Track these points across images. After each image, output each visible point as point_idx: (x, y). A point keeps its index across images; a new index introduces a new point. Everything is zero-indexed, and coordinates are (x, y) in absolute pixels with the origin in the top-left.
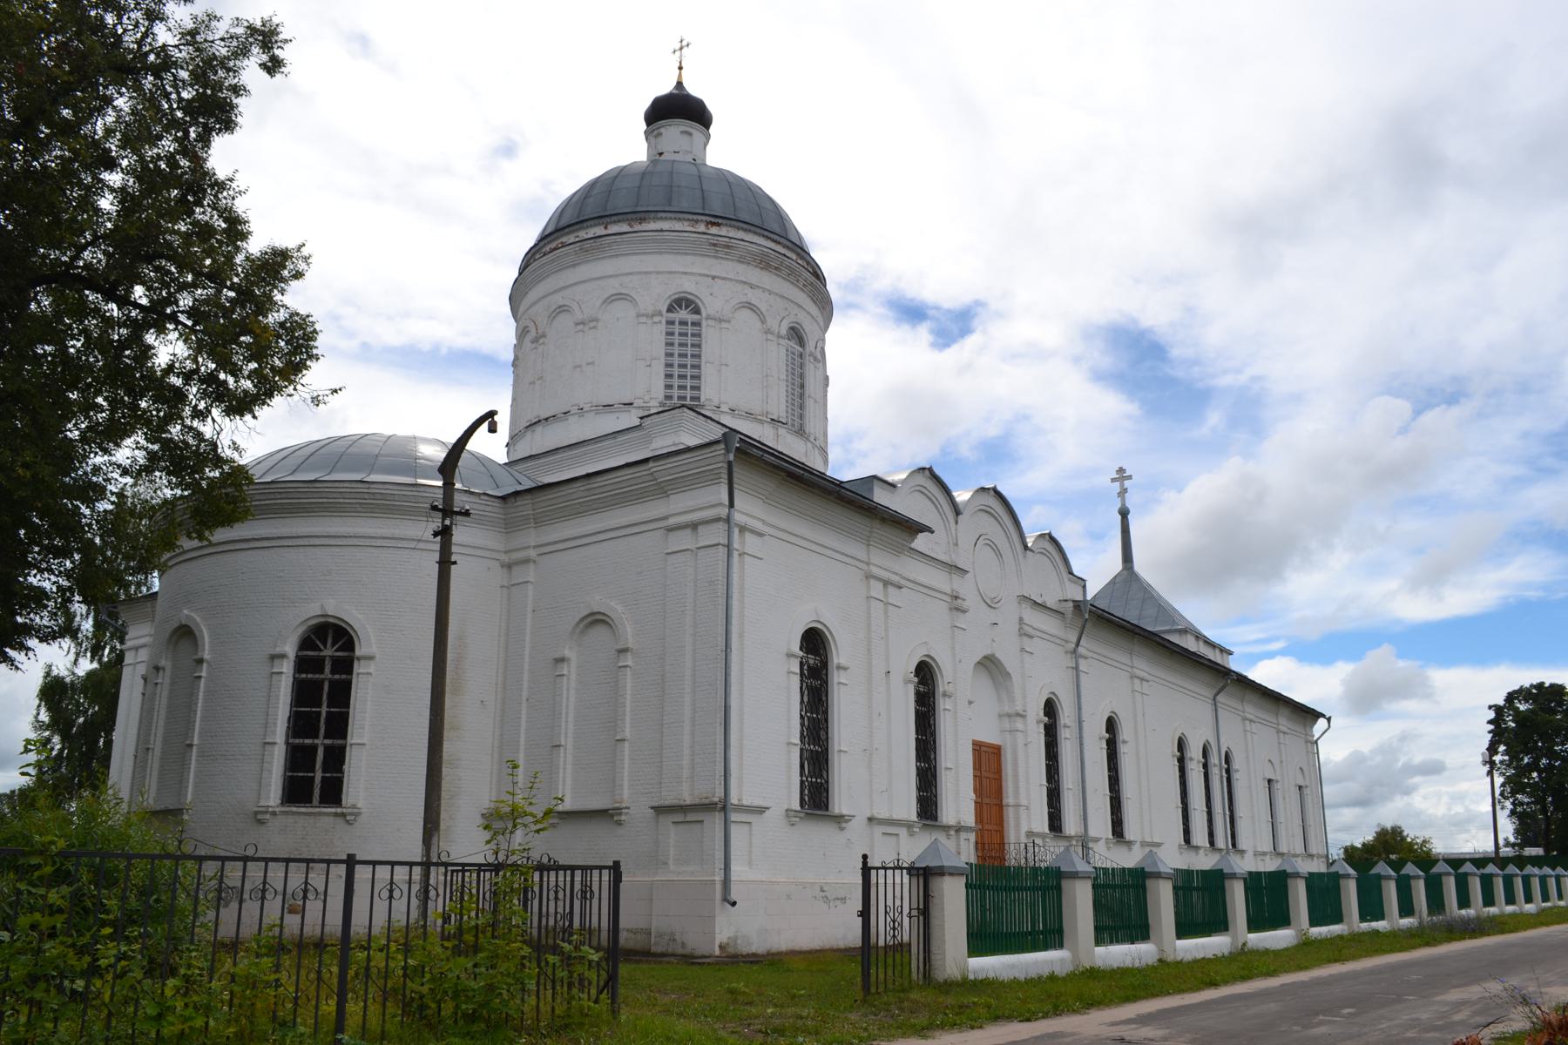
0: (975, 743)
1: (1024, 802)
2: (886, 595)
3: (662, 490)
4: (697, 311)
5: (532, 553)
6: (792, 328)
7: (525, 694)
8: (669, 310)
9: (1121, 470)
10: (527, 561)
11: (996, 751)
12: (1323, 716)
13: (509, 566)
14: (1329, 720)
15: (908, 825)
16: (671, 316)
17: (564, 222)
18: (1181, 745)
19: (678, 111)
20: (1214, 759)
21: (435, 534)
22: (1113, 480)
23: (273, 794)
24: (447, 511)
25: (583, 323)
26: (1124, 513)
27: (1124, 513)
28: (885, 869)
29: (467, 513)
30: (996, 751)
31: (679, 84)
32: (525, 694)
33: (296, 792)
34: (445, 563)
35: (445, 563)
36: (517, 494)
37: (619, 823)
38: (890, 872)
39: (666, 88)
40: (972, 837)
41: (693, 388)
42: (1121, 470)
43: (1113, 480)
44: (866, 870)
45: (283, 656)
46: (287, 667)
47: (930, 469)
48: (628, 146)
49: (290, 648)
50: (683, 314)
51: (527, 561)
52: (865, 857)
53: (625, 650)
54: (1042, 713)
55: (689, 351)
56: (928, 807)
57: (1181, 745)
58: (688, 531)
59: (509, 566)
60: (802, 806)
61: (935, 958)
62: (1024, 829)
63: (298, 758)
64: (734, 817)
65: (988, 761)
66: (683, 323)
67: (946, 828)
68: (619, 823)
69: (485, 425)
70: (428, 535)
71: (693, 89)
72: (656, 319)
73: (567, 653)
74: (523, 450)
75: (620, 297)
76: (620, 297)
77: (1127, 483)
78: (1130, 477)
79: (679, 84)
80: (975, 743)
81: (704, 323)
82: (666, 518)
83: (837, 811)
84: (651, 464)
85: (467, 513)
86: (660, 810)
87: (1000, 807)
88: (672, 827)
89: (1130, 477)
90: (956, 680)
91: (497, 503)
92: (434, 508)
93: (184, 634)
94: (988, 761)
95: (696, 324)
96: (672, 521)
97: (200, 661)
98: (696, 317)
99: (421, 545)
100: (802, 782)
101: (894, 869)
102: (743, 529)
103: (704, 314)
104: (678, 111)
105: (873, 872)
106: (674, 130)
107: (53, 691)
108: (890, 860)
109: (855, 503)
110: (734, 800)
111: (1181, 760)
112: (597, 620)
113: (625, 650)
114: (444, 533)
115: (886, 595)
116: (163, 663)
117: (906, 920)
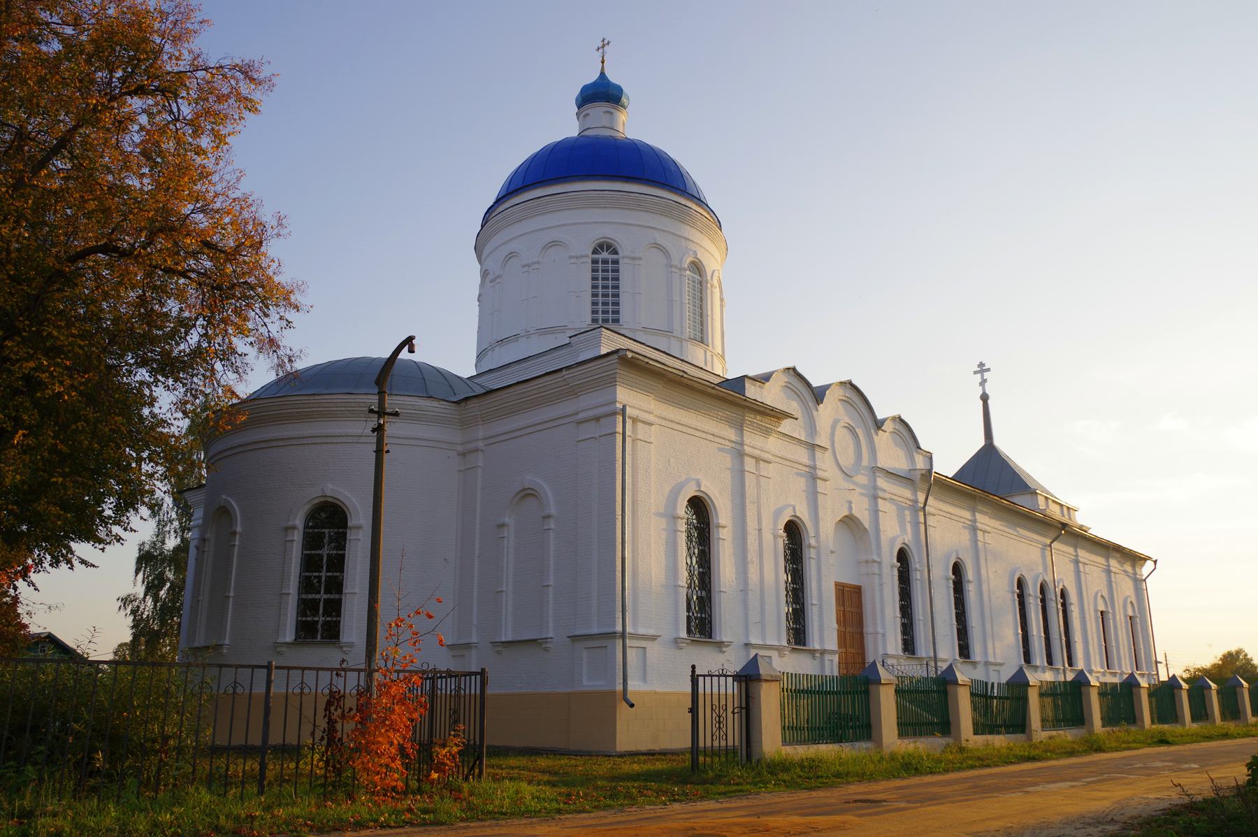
0: (837, 584)
1: (880, 630)
2: (758, 469)
3: (574, 392)
4: (616, 253)
5: (481, 444)
6: (693, 263)
7: (477, 552)
8: (594, 252)
9: (981, 365)
10: (477, 450)
11: (858, 590)
12: (1150, 558)
13: (463, 455)
14: (1155, 562)
15: (779, 649)
16: (596, 256)
17: (512, 188)
18: (1021, 584)
19: (601, 94)
20: (1051, 596)
21: (374, 430)
22: (975, 373)
23: (289, 636)
24: (381, 413)
25: (528, 265)
26: (985, 398)
27: (985, 398)
28: (712, 676)
29: (396, 414)
30: (858, 590)
31: (602, 74)
32: (477, 552)
33: (306, 631)
34: (379, 452)
35: (379, 452)
36: (467, 399)
37: (546, 650)
38: (715, 679)
39: (593, 77)
40: (836, 658)
41: (614, 312)
42: (981, 365)
43: (975, 373)
44: (694, 679)
45: (294, 528)
46: (297, 537)
47: (794, 369)
48: (564, 125)
49: (299, 522)
50: (605, 255)
51: (477, 450)
52: (693, 667)
53: (549, 516)
54: (895, 560)
55: (610, 283)
56: (798, 634)
57: (1021, 584)
58: (593, 423)
59: (463, 455)
60: (689, 631)
61: (754, 745)
62: (881, 652)
63: (306, 607)
64: (628, 642)
65: (851, 600)
66: (605, 262)
67: (812, 652)
68: (546, 650)
69: (406, 348)
70: (368, 431)
71: (613, 77)
72: (583, 260)
73: (507, 520)
74: (487, 365)
75: (555, 243)
76: (555, 243)
77: (986, 375)
78: (988, 370)
79: (602, 74)
80: (837, 584)
81: (621, 262)
82: (577, 413)
83: (718, 639)
84: (564, 372)
85: (396, 414)
86: (574, 638)
87: (861, 635)
88: (585, 653)
89: (988, 370)
90: (823, 536)
91: (453, 407)
92: (371, 411)
93: (223, 513)
94: (851, 600)
95: (616, 262)
96: (581, 416)
97: (234, 533)
98: (615, 257)
99: (363, 440)
100: (688, 617)
101: (719, 676)
102: (635, 420)
103: (621, 254)
104: (601, 94)
105: (701, 679)
106: (598, 110)
107: (146, 559)
108: (715, 669)
109: (731, 397)
110: (629, 629)
111: (1021, 597)
112: (528, 494)
113: (549, 516)
114: (379, 429)
115: (758, 469)
116: (208, 536)
117: (730, 715)
